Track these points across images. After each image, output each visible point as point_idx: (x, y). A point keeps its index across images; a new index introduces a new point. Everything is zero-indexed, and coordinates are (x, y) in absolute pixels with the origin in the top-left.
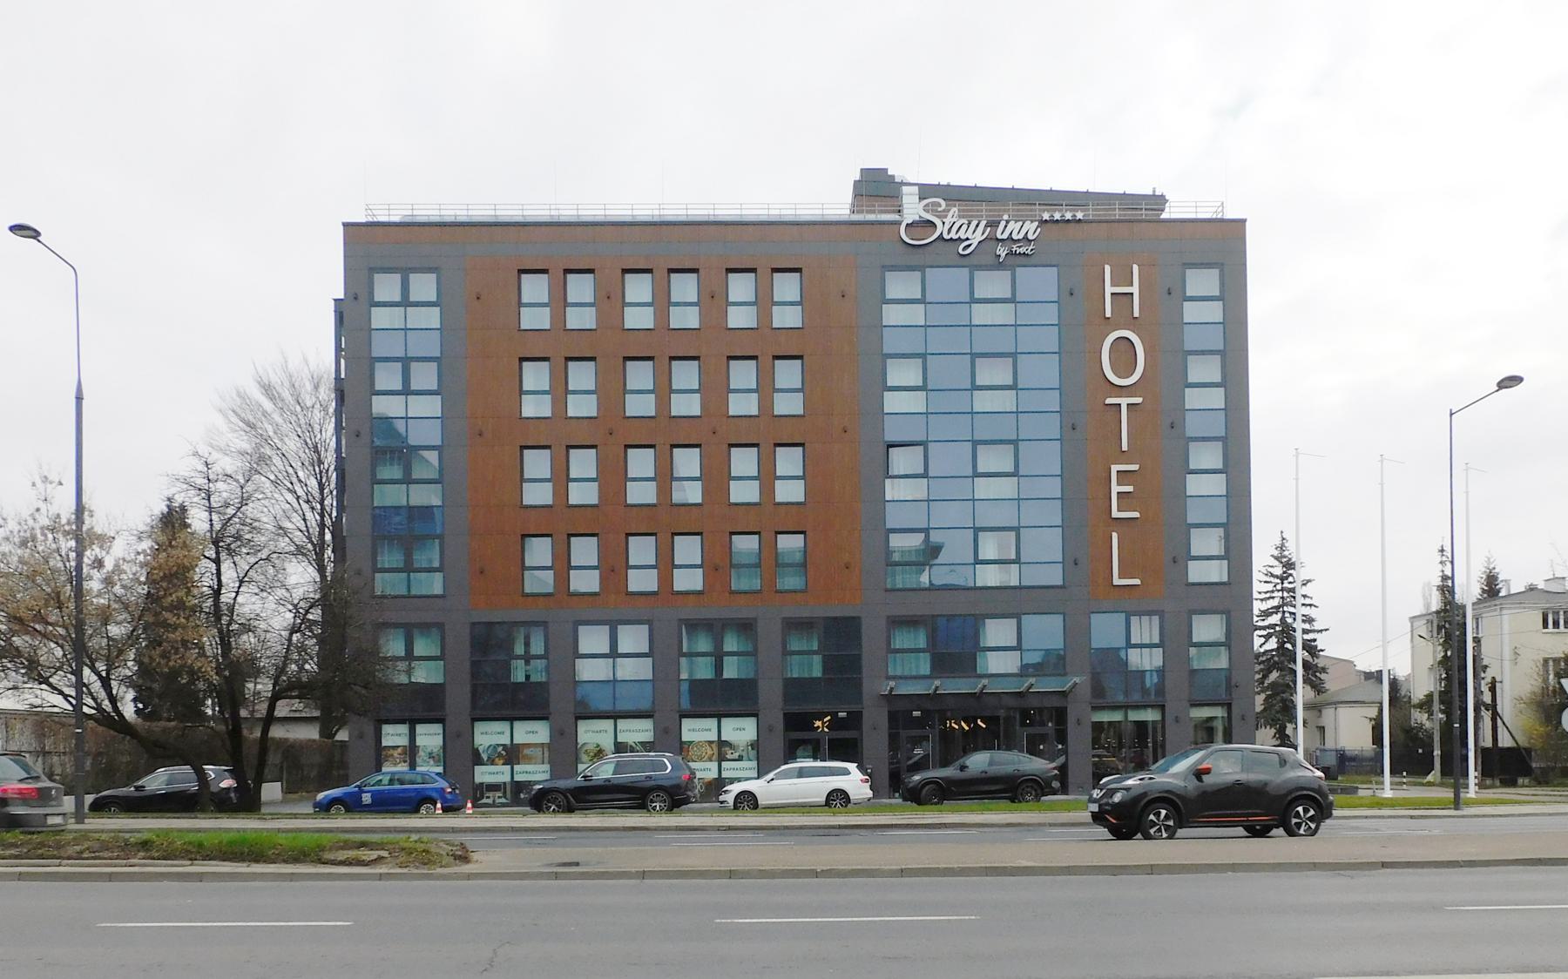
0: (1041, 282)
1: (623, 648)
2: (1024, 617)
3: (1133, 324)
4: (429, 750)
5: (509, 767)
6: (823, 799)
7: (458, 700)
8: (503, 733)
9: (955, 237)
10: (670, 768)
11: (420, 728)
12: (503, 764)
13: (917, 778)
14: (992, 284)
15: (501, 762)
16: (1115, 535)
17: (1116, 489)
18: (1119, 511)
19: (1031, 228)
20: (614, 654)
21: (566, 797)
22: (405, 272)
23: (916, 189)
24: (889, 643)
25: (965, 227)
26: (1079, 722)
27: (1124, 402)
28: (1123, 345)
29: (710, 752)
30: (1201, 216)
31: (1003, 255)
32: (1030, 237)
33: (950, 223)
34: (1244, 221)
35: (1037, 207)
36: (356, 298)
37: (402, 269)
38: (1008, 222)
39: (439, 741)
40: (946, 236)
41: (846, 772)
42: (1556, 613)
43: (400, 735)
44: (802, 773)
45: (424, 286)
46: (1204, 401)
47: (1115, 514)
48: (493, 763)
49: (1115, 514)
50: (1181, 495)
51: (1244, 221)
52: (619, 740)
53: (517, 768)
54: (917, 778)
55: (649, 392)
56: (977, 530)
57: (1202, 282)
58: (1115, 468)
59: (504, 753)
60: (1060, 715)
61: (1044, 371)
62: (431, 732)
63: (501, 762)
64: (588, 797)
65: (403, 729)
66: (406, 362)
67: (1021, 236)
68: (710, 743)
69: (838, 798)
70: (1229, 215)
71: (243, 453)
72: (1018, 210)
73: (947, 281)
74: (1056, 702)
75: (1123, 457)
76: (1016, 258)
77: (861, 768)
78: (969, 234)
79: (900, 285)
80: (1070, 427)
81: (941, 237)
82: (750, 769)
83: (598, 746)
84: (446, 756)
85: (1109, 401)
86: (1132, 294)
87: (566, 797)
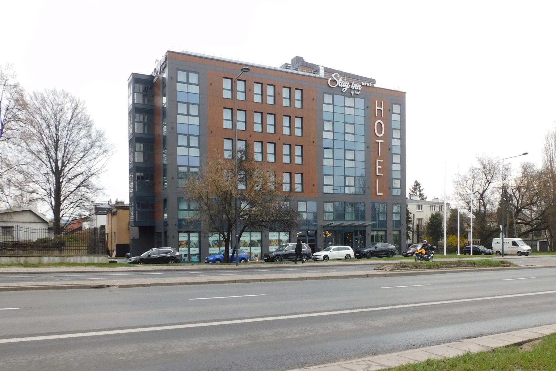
0: (360, 103)
1: (191, 208)
2: (308, 202)
3: (381, 118)
4: (194, 242)
5: (219, 248)
6: (344, 257)
7: (204, 226)
8: (276, 236)
9: (342, 86)
10: (306, 248)
11: (191, 234)
12: (217, 247)
13: (366, 250)
14: (349, 102)
15: (216, 246)
16: (377, 180)
17: (378, 167)
18: (378, 173)
19: (359, 87)
20: (189, 209)
21: (281, 257)
22: (188, 72)
23: (323, 68)
24: (178, 207)
25: (344, 83)
26: (368, 234)
27: (380, 141)
28: (379, 124)
29: (276, 243)
30: (383, 87)
31: (353, 94)
32: (359, 89)
33: (340, 82)
34: (405, 93)
35: (345, 78)
36: (313, 100)
37: (187, 71)
38: (354, 84)
39: (197, 239)
40: (339, 86)
41: (349, 249)
42: (419, 206)
43: (185, 237)
44: (339, 249)
45: (194, 78)
46: (396, 143)
47: (378, 174)
48: (214, 247)
49: (378, 174)
50: (322, 165)
51: (405, 93)
52: (251, 239)
53: (221, 248)
54: (366, 250)
55: (284, 126)
56: (345, 176)
57: (396, 109)
58: (378, 161)
59: (217, 243)
60: (363, 233)
61: (361, 130)
62: (195, 236)
63: (216, 246)
64: (289, 257)
65: (186, 235)
66: (188, 104)
67: (353, 88)
68: (276, 240)
69: (348, 256)
70: (400, 90)
71: (101, 131)
72: (348, 79)
73: (339, 99)
74: (362, 229)
75: (379, 157)
76: (350, 94)
77: (352, 247)
78: (345, 86)
79: (328, 99)
80: (367, 147)
81: (338, 86)
82: (186, 251)
83: (245, 241)
84: (269, 243)
85: (376, 141)
86: (381, 110)
87: (281, 257)
